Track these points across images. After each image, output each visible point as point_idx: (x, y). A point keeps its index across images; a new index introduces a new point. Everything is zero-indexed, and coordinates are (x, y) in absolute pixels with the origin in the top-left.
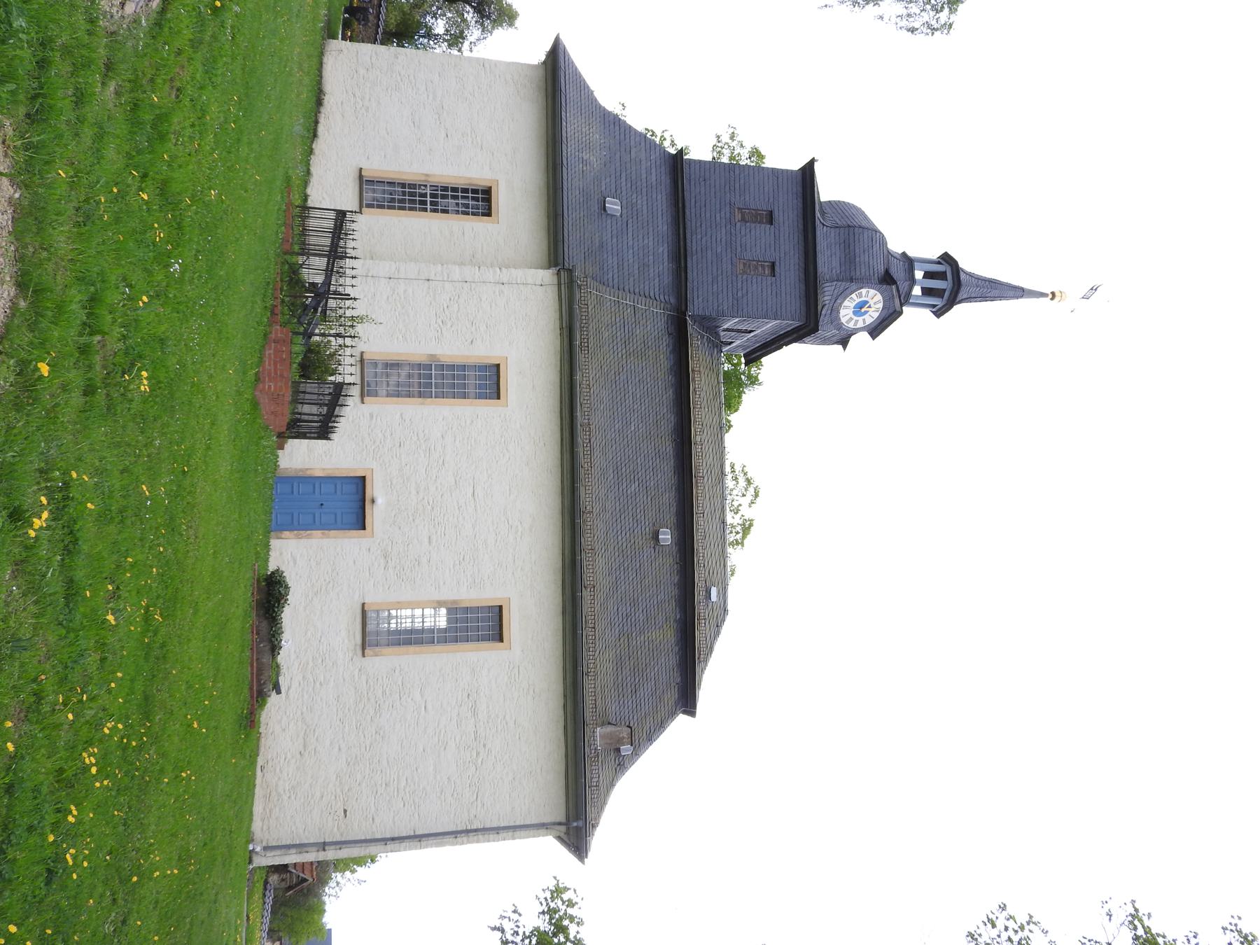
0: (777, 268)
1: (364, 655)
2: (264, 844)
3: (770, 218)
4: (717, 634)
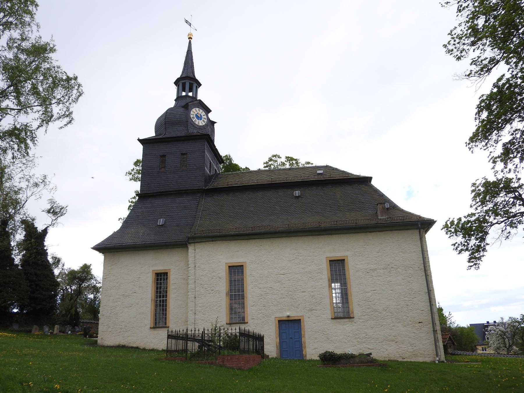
0: (184, 152)
1: (353, 318)
2: (435, 356)
3: (163, 156)
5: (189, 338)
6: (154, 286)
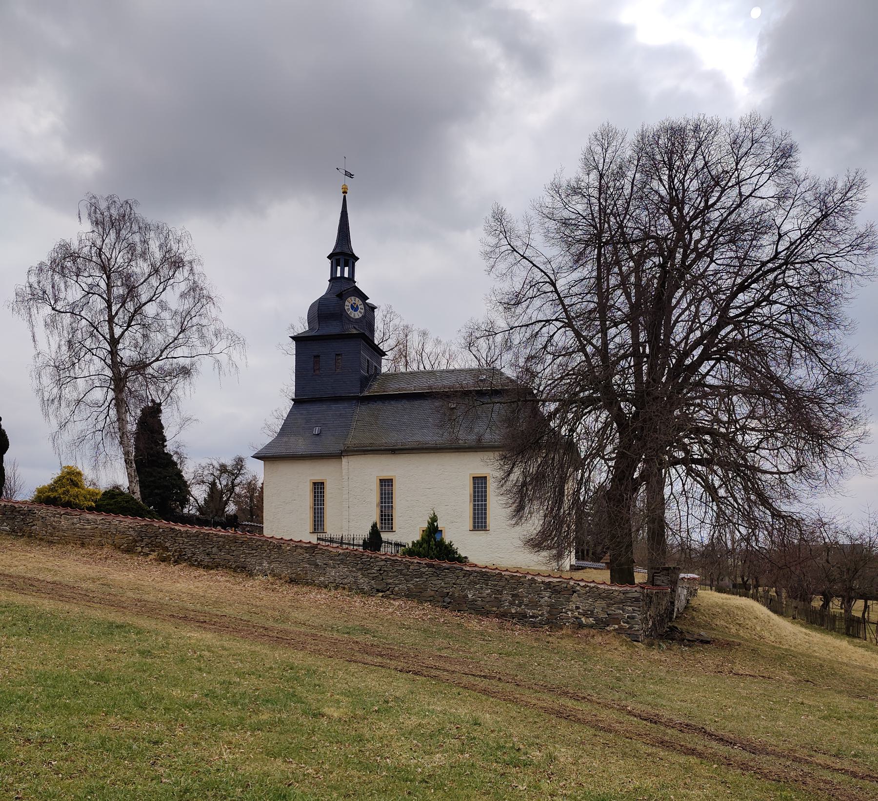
6: (312, 495)
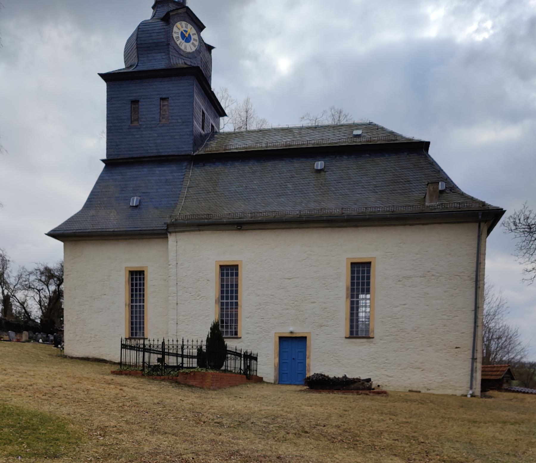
0: (164, 96)
1: (373, 338)
2: (469, 389)
3: (135, 102)
4: (382, 129)
5: (147, 349)
